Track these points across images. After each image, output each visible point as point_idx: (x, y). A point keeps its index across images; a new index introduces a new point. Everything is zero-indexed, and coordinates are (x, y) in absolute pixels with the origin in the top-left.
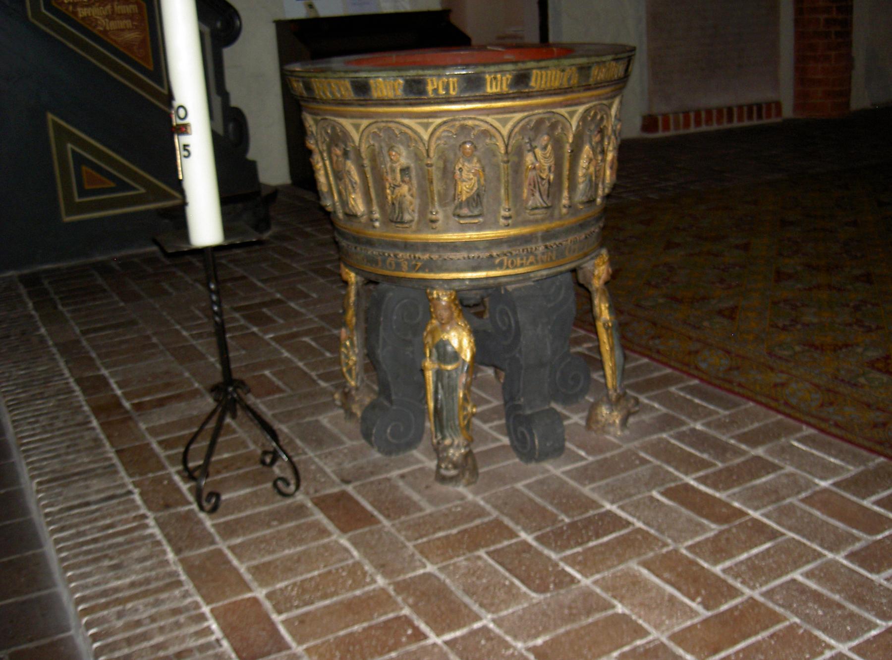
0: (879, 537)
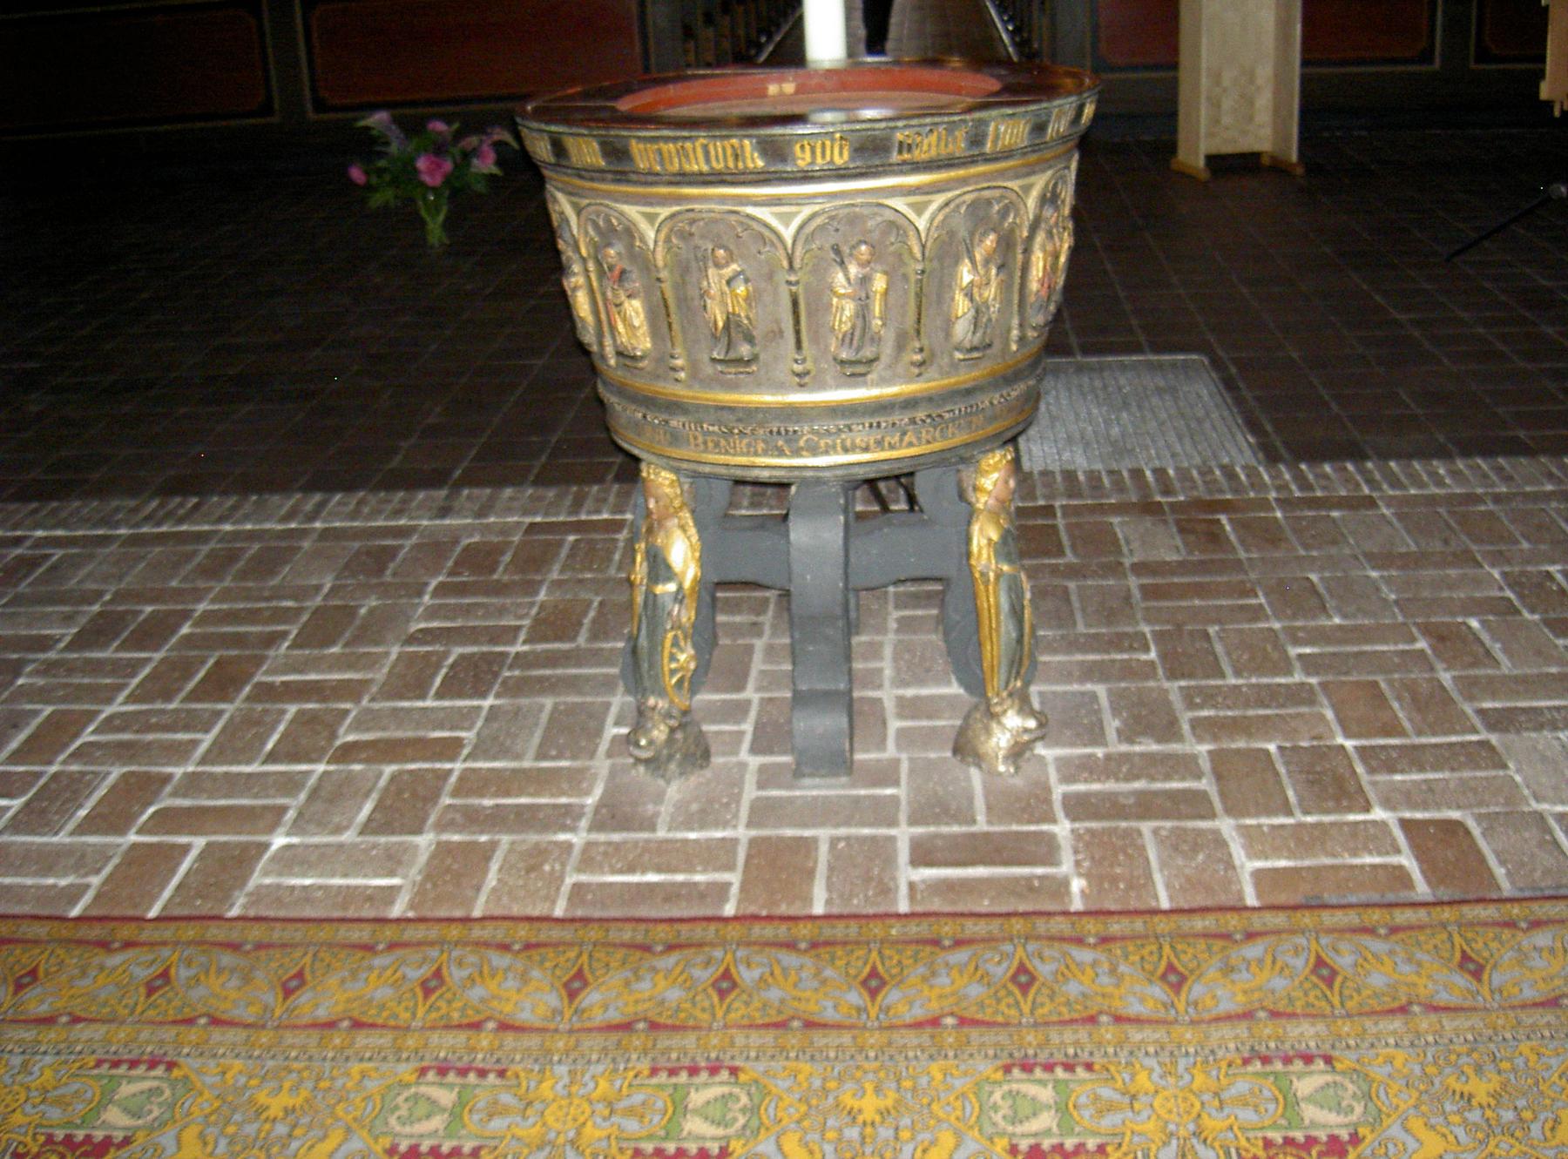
0: (151, 810)
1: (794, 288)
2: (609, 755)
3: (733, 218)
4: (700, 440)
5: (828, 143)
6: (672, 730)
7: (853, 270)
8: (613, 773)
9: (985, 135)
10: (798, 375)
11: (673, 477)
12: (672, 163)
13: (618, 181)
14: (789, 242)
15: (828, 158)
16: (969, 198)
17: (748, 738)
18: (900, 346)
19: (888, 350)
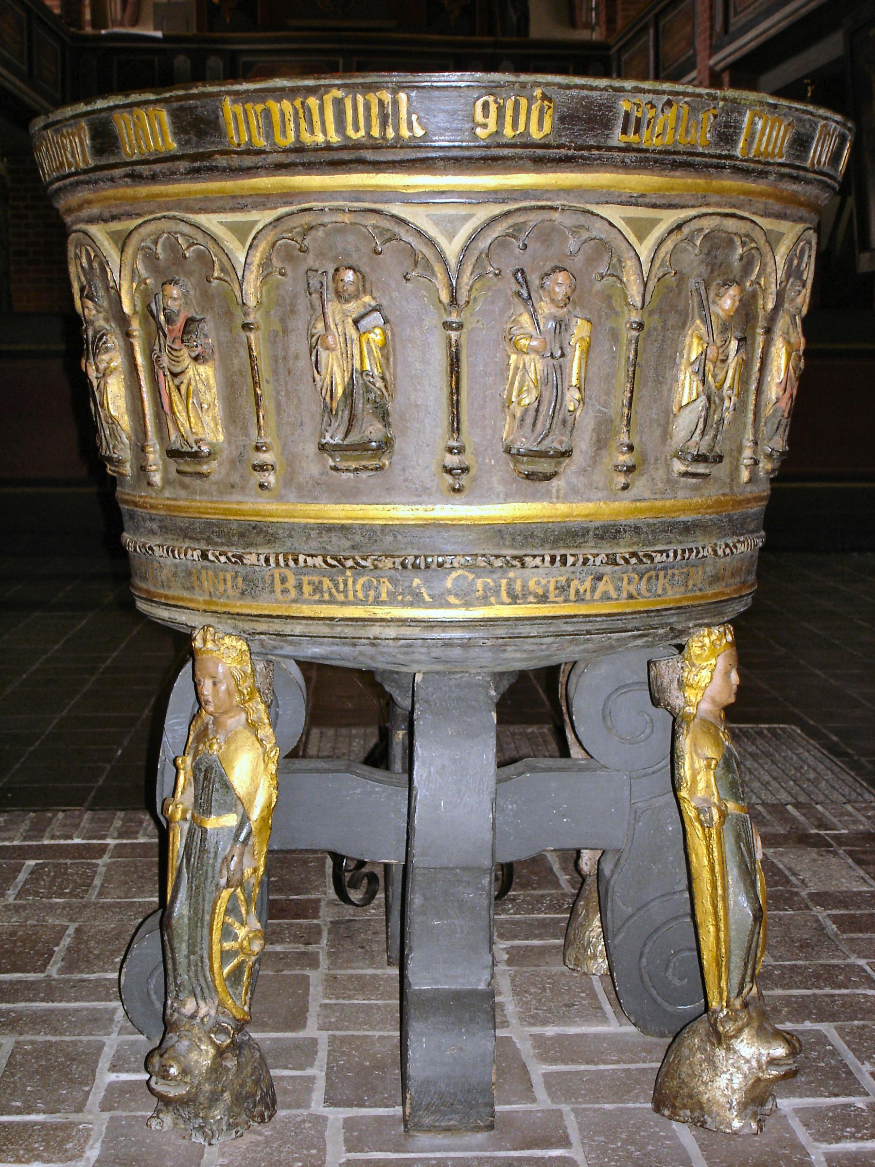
1: (454, 335)
2: (106, 1106)
3: (372, 220)
4: (292, 581)
5: (524, 102)
6: (220, 1052)
7: (545, 308)
8: (114, 1130)
9: (738, 128)
10: (449, 471)
11: (242, 645)
12: (284, 133)
13: (194, 173)
14: (453, 261)
15: (521, 128)
16: (708, 224)
17: (321, 1085)
18: (601, 443)
19: (583, 445)
